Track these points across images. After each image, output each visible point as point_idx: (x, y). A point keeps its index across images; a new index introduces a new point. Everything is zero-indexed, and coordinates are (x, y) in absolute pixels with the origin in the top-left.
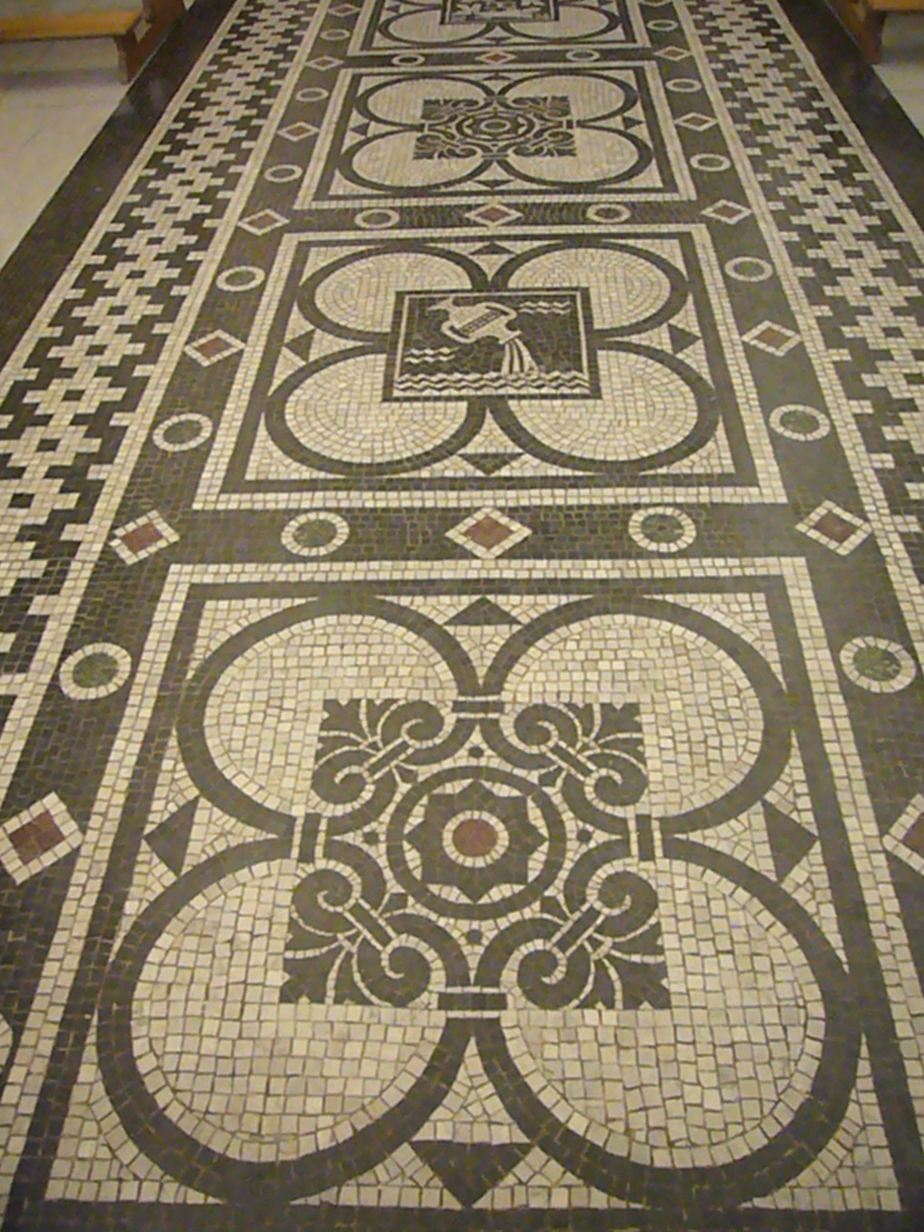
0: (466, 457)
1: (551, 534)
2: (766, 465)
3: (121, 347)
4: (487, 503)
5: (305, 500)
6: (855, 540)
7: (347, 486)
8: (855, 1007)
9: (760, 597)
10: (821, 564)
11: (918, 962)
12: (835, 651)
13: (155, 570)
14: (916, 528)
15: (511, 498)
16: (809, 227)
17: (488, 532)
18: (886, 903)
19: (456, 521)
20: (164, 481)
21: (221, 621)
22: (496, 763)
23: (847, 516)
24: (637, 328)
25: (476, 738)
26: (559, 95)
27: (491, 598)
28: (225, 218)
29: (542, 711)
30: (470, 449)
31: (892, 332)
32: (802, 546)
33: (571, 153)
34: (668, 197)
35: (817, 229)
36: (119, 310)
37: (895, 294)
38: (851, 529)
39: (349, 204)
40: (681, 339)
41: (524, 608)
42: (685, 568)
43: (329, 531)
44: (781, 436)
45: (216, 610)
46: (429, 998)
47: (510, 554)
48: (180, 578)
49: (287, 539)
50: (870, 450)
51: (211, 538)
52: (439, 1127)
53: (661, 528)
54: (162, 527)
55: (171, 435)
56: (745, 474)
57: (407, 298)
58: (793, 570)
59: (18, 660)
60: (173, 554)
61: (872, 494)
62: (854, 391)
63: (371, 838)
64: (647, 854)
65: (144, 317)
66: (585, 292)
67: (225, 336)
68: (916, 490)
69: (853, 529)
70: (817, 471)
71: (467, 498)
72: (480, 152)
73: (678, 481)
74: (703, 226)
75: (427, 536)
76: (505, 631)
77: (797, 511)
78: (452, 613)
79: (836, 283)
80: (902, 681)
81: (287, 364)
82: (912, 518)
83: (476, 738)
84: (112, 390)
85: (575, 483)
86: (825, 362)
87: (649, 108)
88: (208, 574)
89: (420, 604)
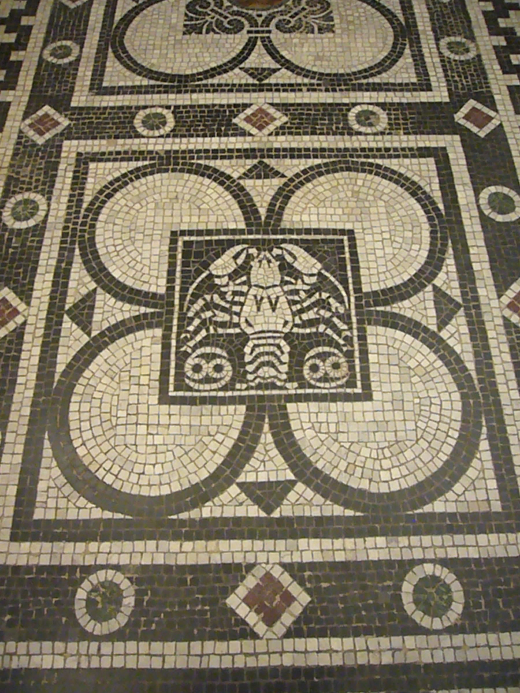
0: (246, 70)
1: (303, 119)
4: (260, 100)
5: (142, 99)
8: (481, 404)
9: (431, 160)
10: (470, 143)
11: (518, 374)
12: (477, 193)
13: (53, 149)
18: (510, 383)
21: (100, 174)
25: (260, 20)
29: (227, 31)
33: (331, 29)
34: (423, 97)
41: (292, 167)
46: (245, 31)
47: (246, 106)
48: (71, 148)
49: (137, 122)
51: (89, 123)
54: (57, 117)
56: (425, 85)
58: (453, 145)
59: (10, 83)
62: (494, 30)
66: (351, 232)
68: (516, 59)
69: (490, 119)
70: (469, 83)
72: (247, 27)
74: (457, 138)
75: (219, 121)
77: (457, 101)
78: (242, 171)
79: (507, 16)
81: (72, 338)
82: (515, 76)
83: (260, 20)
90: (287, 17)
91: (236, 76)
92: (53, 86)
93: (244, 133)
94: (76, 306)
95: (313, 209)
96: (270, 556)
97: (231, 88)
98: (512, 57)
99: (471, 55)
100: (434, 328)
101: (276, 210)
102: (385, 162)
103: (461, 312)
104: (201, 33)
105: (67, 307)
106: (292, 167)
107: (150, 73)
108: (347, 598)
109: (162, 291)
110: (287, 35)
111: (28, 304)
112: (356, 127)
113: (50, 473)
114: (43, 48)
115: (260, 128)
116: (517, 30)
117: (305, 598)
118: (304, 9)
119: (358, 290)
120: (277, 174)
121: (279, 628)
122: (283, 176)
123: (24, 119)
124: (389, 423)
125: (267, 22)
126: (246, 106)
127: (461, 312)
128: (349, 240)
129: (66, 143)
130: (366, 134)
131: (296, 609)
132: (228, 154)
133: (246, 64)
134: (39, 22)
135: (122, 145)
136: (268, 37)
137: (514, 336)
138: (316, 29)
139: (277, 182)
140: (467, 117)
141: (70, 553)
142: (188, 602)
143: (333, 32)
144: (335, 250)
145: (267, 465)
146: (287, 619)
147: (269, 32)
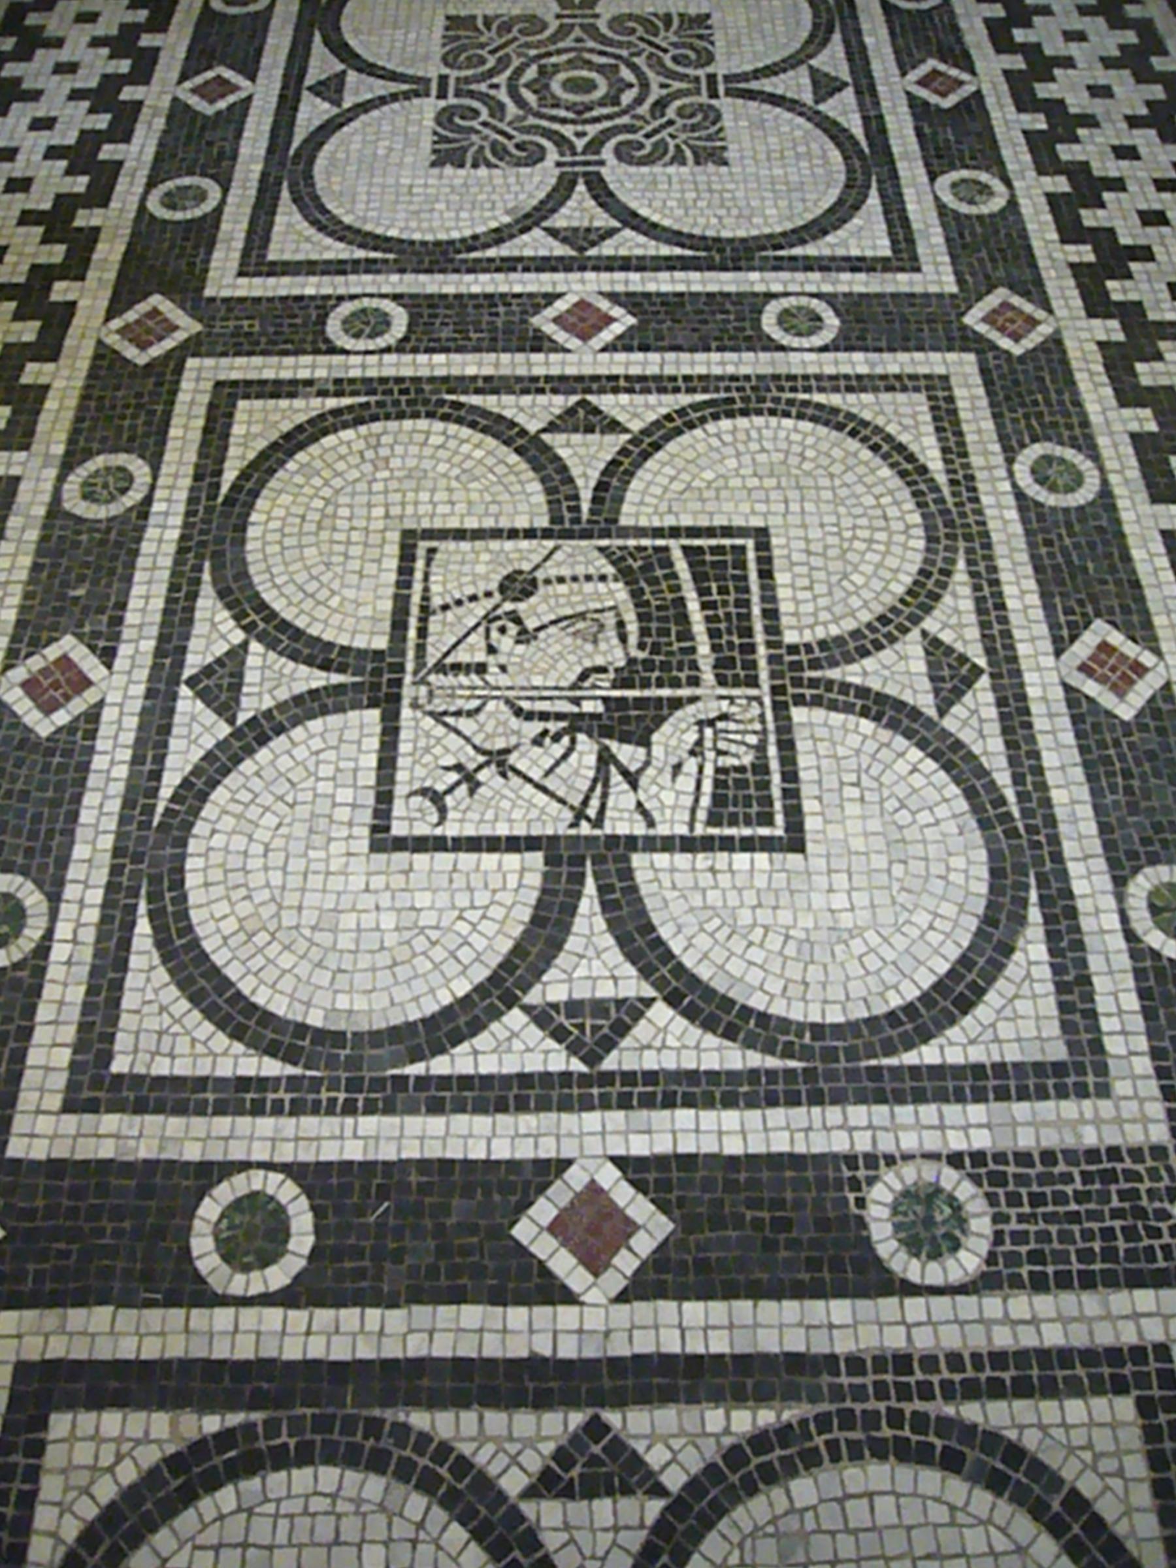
0: (553, 232)
1: (658, 324)
2: (931, 241)
3: (97, 65)
4: (578, 287)
9: (921, 397)
15: (622, 282)
16: (1038, 46)
17: (584, 322)
19: (537, 309)
20: (165, 259)
21: (254, 426)
22: (591, 44)
23: (1028, 308)
24: (771, 71)
25: (580, 144)
26: (693, 11)
28: (114, 204)
30: (559, 221)
31: (1100, 91)
32: (968, 341)
34: (902, 282)
35: (1048, 51)
36: (70, 68)
37: (1132, 96)
39: (311, 286)
40: (825, 86)
41: (637, 412)
42: (830, 364)
43: (384, 322)
44: (956, 215)
47: (551, 298)
48: (198, 379)
49: (333, 327)
50: (1041, 171)
52: (553, 988)
53: (801, 322)
55: (170, 201)
56: (904, 255)
57: (423, 545)
58: (961, 368)
60: (194, 347)
63: (496, 86)
64: (714, 94)
65: (106, 77)
66: (762, 536)
67: (228, 74)
69: (1033, 322)
70: (992, 251)
72: (552, 155)
75: (508, 325)
77: (969, 295)
81: (197, 728)
83: (580, 144)
84: (18, 326)
86: (1010, 125)
87: (857, 55)
88: (240, 368)
89: (506, 405)
90: (638, 137)
91: (535, 243)
95: (694, 483)
96: (592, 1144)
100: (932, 712)
103: (984, 681)
104: (461, 165)
108: (758, 1227)
110: (633, 169)
113: (146, 975)
114: (146, 192)
115: (584, 337)
118: (671, 123)
121: (613, 1282)
122: (626, 430)
123: (108, 319)
124: (859, 893)
125: (595, 146)
126: (551, 298)
128: (758, 548)
129: (191, 363)
132: (531, 385)
133: (559, 221)
134: (174, 44)
135: (302, 367)
140: (988, 319)
141: (186, 1138)
144: (731, 565)
145: (592, 964)
146: (626, 1263)
147: (602, 163)
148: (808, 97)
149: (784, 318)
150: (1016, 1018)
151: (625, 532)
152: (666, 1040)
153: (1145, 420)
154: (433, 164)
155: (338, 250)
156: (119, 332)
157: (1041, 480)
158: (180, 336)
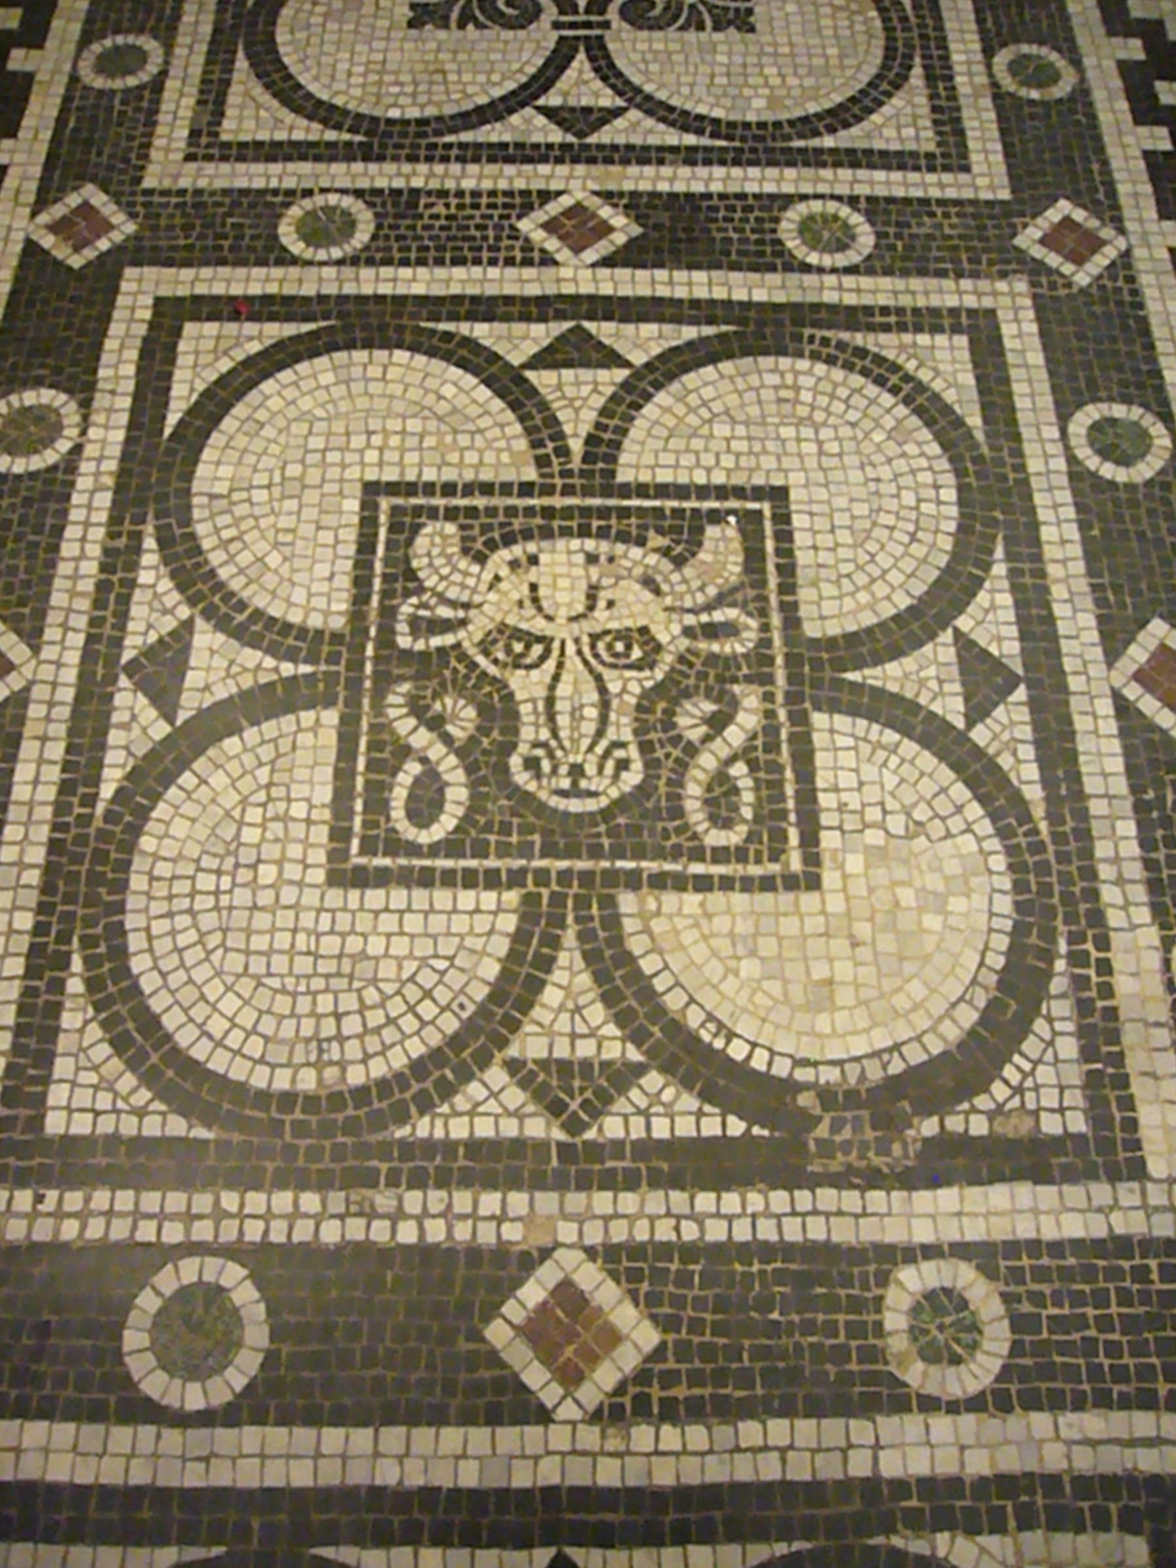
0: (549, 113)
1: (674, 231)
4: (576, 184)
6: (1100, 261)
7: (367, 154)
8: (1052, 897)
13: (103, 279)
14: (1166, 145)
17: (578, 228)
19: (527, 208)
27: (587, 325)
30: (552, 99)
38: (1095, 244)
41: (642, 342)
45: (200, 337)
47: (546, 196)
48: (139, 292)
50: (1111, 33)
53: (827, 234)
56: (952, 155)
61: (1133, 187)
66: (779, 495)
68: (1169, 93)
70: (1054, 150)
71: (542, 175)
73: (853, 158)
74: (1021, 285)
75: (478, 231)
76: (611, 378)
80: (1145, 470)
82: (1163, 131)
85: (709, 157)
88: (184, 281)
92: (100, 141)
93: (547, 260)
94: (149, 652)
97: (500, 153)
98: (1160, 86)
99: (1061, 90)
101: (604, 445)
102: (672, 138)
105: (127, 656)
106: (642, 342)
107: (326, 113)
109: (338, 623)
111: (36, 649)
112: (297, 247)
115: (577, 250)
116: (1168, 25)
117: (648, 1336)
119: (792, 622)
120: (613, 359)
124: (860, 938)
127: (1021, 693)
128: (775, 518)
129: (130, 272)
130: (821, 270)
131: (628, 1359)
133: (552, 99)
135: (256, 281)
136: (600, 38)
137: (1161, 855)
138: (709, 23)
139: (611, 378)
142: (386, 1338)
143: (752, 29)
148: (951, 707)
149: (808, 229)
150: (1044, 1082)
151: (625, 491)
152: (668, 1111)
153: (1160, 139)
154: (411, 24)
155: (303, 130)
156: (611, 229)
157: (1105, 453)
158: (117, 237)
